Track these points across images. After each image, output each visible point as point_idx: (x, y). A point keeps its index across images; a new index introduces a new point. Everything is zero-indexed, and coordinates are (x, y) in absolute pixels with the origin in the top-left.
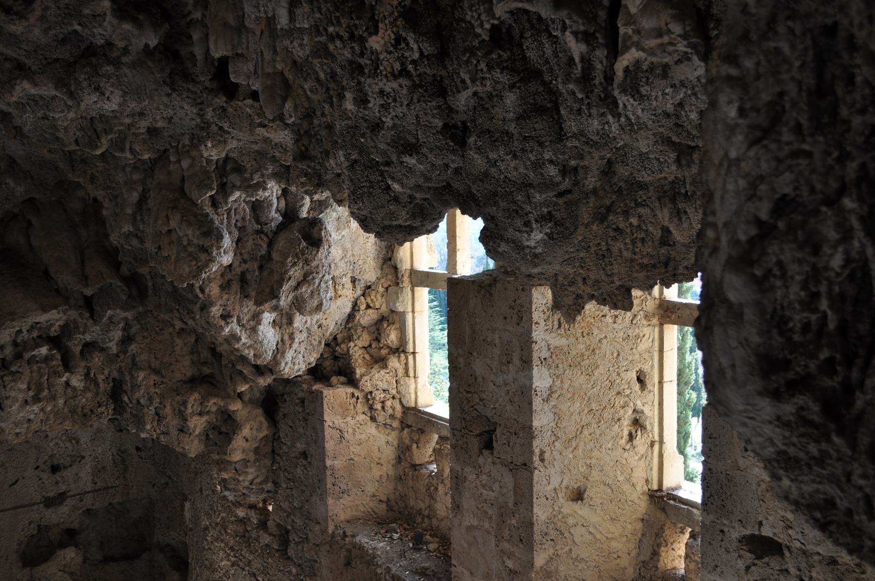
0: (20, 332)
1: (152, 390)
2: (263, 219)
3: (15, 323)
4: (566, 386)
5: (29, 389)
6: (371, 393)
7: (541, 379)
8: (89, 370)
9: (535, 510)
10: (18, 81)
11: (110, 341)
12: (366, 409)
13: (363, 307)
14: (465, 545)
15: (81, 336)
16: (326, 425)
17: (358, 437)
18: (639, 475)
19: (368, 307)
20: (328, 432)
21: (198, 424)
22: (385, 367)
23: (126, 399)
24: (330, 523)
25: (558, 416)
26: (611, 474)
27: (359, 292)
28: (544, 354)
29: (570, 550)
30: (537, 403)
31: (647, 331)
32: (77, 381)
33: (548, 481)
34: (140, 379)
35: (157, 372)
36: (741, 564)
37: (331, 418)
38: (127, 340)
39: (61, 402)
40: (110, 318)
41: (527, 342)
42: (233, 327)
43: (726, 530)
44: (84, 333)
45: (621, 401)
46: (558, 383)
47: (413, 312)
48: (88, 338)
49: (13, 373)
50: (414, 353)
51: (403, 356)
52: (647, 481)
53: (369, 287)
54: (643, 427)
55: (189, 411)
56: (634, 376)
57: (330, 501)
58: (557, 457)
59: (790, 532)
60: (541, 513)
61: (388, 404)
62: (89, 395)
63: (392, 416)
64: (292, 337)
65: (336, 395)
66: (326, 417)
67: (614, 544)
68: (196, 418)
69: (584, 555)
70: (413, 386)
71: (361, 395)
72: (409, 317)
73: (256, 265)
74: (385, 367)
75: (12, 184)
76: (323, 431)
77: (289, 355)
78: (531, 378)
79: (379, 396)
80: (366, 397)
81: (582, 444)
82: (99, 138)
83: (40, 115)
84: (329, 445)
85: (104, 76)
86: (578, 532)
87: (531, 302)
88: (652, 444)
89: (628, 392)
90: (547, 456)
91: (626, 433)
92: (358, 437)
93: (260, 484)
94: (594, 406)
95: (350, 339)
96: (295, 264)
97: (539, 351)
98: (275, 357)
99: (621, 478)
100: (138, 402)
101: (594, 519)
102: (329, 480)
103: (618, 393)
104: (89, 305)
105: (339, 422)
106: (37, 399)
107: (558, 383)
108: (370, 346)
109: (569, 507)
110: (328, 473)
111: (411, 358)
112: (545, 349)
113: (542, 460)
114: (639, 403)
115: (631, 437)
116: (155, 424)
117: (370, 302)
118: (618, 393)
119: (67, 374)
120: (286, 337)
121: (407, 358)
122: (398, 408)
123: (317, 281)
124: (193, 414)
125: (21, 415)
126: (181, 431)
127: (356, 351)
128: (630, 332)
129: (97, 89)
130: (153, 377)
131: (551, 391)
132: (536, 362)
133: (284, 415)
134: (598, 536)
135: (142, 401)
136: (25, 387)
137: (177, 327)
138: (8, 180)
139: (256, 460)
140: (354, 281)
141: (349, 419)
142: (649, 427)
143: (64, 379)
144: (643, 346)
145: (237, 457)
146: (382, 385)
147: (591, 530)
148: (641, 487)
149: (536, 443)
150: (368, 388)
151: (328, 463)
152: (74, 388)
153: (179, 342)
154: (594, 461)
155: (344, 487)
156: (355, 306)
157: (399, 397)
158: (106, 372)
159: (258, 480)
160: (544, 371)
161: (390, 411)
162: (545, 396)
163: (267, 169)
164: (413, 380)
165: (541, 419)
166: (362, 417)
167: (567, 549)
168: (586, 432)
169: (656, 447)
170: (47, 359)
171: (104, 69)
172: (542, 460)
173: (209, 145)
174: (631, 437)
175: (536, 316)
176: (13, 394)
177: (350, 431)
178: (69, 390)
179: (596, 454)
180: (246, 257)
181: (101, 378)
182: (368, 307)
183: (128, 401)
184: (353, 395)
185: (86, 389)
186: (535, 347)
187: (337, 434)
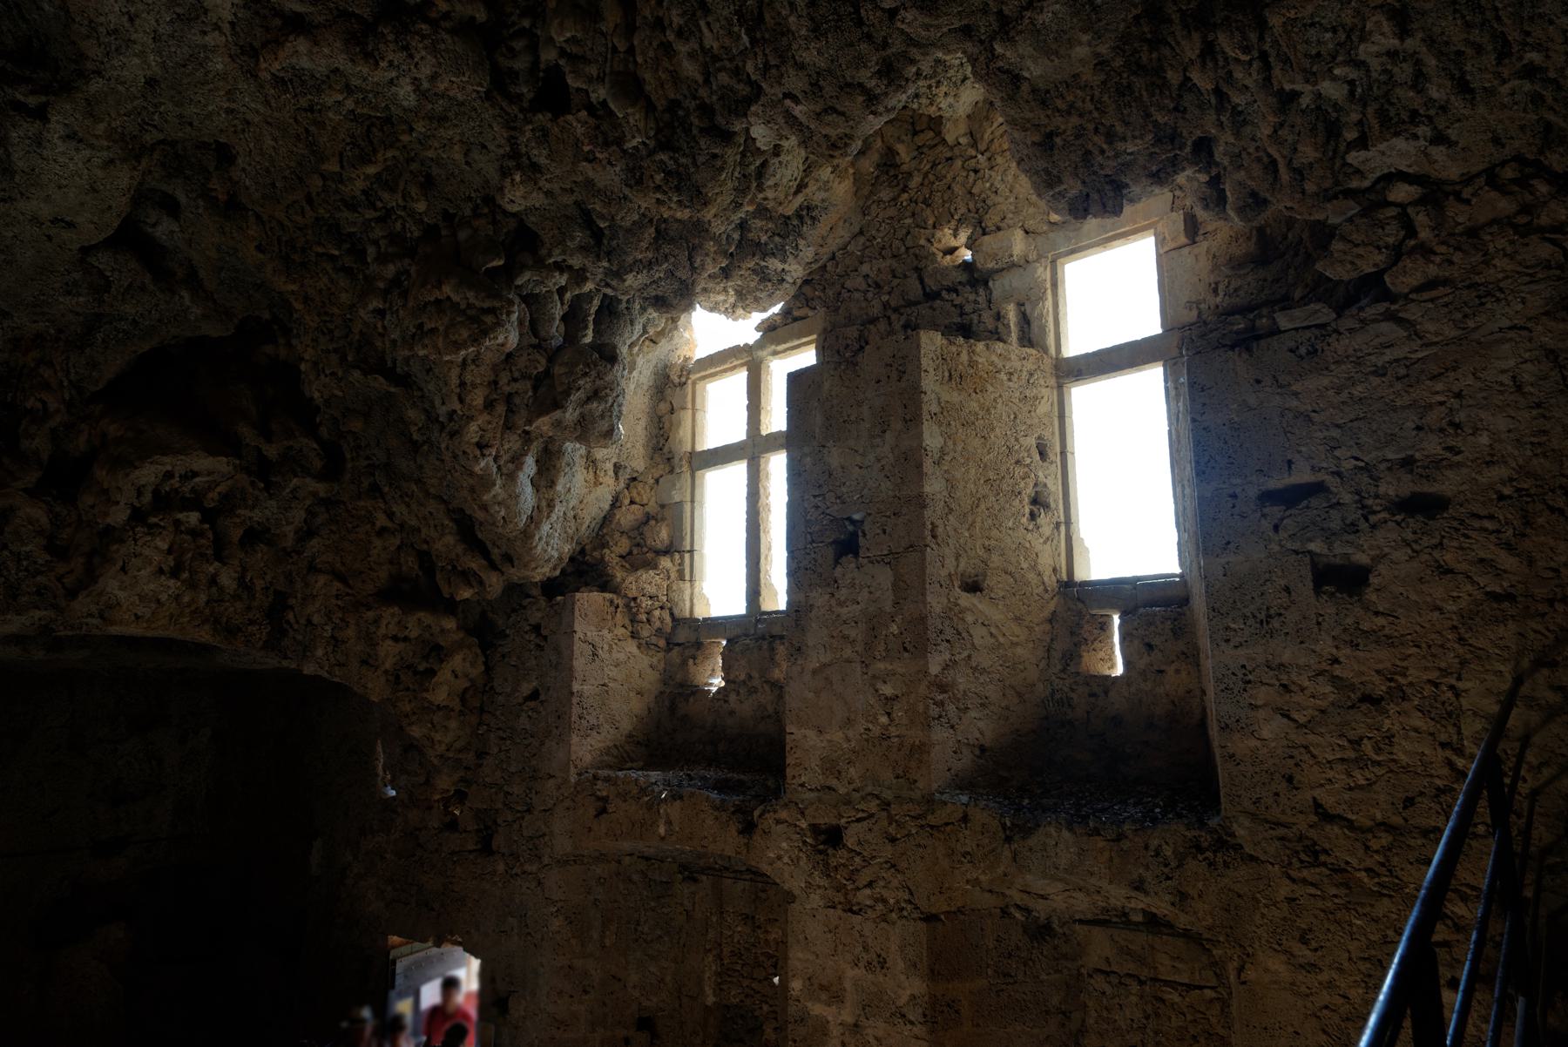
0: (169, 475)
1: (334, 601)
2: (543, 334)
3: (167, 459)
4: (959, 448)
5: (170, 551)
6: (635, 599)
7: (932, 438)
8: (244, 570)
9: (929, 599)
10: (291, 38)
11: (288, 523)
12: (627, 622)
13: (627, 502)
14: (811, 695)
15: (247, 513)
16: (577, 636)
17: (615, 655)
18: (1045, 562)
19: (632, 502)
20: (578, 647)
21: (389, 653)
22: (655, 567)
23: (291, 616)
24: (573, 770)
25: (951, 483)
26: (1013, 560)
27: (622, 485)
28: (935, 408)
29: (969, 657)
30: (928, 465)
31: (1046, 392)
32: (227, 579)
33: (943, 563)
34: (320, 584)
35: (342, 578)
36: (1266, 525)
37: (583, 628)
38: (306, 533)
39: (203, 598)
40: (295, 490)
41: (916, 391)
42: (485, 464)
43: (1238, 490)
44: (253, 508)
45: (1019, 471)
46: (950, 443)
47: (693, 501)
48: (257, 515)
49: (151, 526)
50: (691, 551)
51: (677, 556)
52: (1055, 570)
53: (634, 479)
54: (1046, 506)
55: (382, 631)
56: (1034, 442)
57: (575, 739)
58: (952, 533)
59: (1337, 453)
60: (936, 602)
61: (657, 613)
62: (239, 605)
63: (659, 630)
64: (551, 506)
65: (589, 601)
66: (577, 627)
67: (1019, 651)
68: (389, 642)
69: (986, 664)
70: (688, 592)
71: (620, 601)
72: (688, 507)
73: (528, 384)
74: (655, 567)
75: (187, 302)
76: (571, 646)
77: (545, 528)
78: (920, 436)
79: (646, 603)
80: (627, 606)
81: (979, 520)
82: (375, 151)
83: (304, 102)
84: (579, 663)
85: (417, 33)
86: (978, 633)
87: (919, 346)
88: (1058, 525)
89: (1028, 461)
90: (940, 530)
91: (1027, 511)
92: (615, 655)
93: (460, 751)
94: (991, 475)
95: (604, 545)
96: (586, 374)
97: (930, 405)
98: (527, 526)
99: (1025, 565)
100: (309, 622)
101: (996, 615)
102: (576, 711)
103: (1017, 462)
104: (263, 471)
105: (592, 634)
106: (175, 573)
107: (950, 443)
108: (630, 553)
109: (966, 599)
110: (575, 700)
111: (687, 556)
112: (935, 402)
113: (934, 537)
114: (1040, 474)
115: (1033, 516)
116: (330, 649)
117: (634, 494)
118: (1017, 462)
119: (217, 564)
120: (544, 504)
121: (682, 558)
122: (668, 619)
123: (610, 400)
124: (385, 637)
125: (152, 586)
126: (364, 662)
127: (611, 557)
128: (1028, 393)
129: (406, 48)
130: (337, 585)
131: (943, 452)
132: (926, 416)
133: (503, 656)
134: (1002, 640)
135: (316, 619)
136: (166, 547)
137: (378, 524)
138: (185, 294)
139: (461, 713)
140: (617, 468)
141: (605, 632)
142: (1053, 505)
143: (211, 569)
144: (1043, 408)
145: (440, 696)
146: (651, 590)
147: (993, 630)
148: (1051, 581)
149: (928, 513)
150: (633, 593)
151: (576, 687)
152: (221, 589)
153: (378, 542)
154: (993, 542)
155: (593, 721)
156: (616, 503)
157: (669, 608)
158: (268, 578)
159: (458, 745)
160: (935, 428)
161: (658, 624)
162: (936, 457)
163: (573, 238)
164: (688, 584)
165: (933, 486)
166: (620, 631)
167: (965, 654)
168: (983, 506)
169: (1063, 528)
170: (195, 533)
171: (418, 26)
172: (934, 537)
173: (518, 178)
174: (1033, 516)
175: (925, 362)
176: (147, 552)
177: (606, 647)
178: (214, 590)
179: (995, 533)
180: (516, 375)
181: (259, 584)
182: (632, 502)
183: (292, 620)
184: (612, 602)
185: (236, 597)
186: (925, 398)
187: (588, 649)
